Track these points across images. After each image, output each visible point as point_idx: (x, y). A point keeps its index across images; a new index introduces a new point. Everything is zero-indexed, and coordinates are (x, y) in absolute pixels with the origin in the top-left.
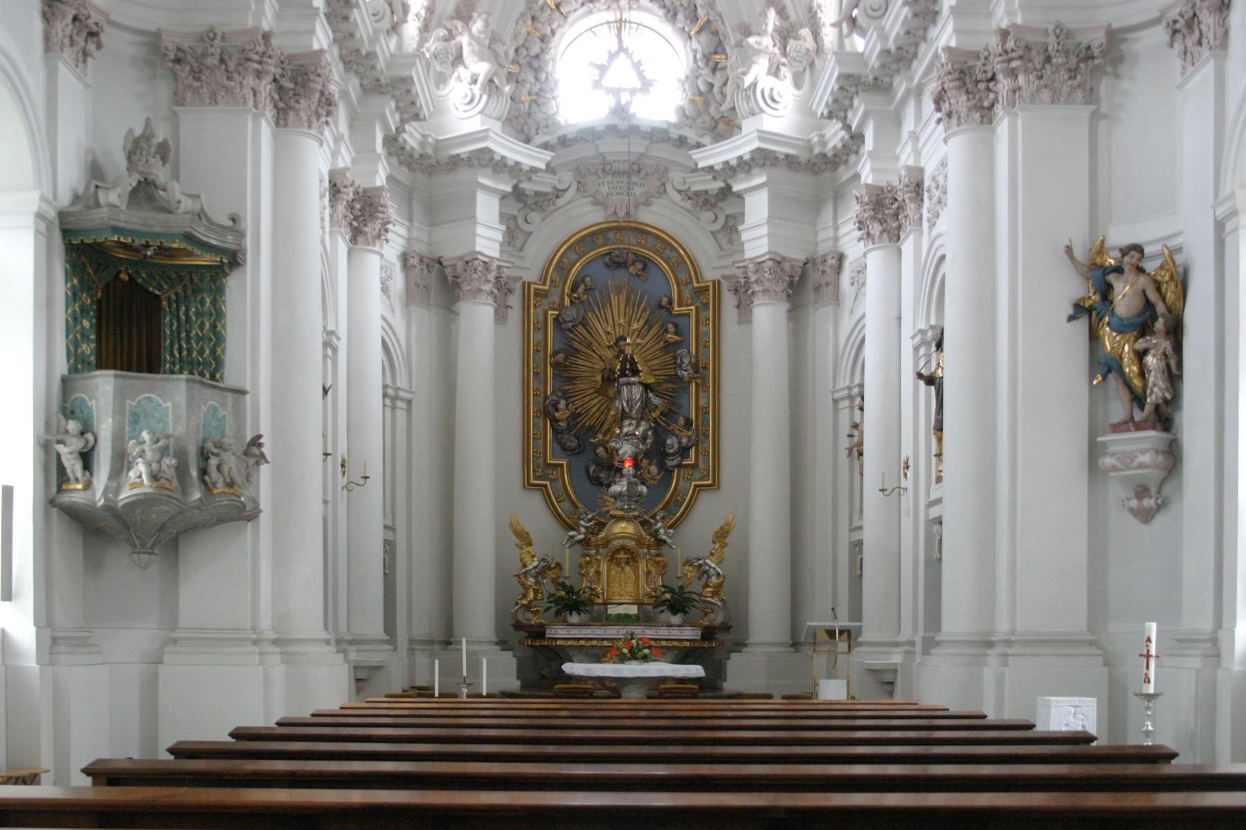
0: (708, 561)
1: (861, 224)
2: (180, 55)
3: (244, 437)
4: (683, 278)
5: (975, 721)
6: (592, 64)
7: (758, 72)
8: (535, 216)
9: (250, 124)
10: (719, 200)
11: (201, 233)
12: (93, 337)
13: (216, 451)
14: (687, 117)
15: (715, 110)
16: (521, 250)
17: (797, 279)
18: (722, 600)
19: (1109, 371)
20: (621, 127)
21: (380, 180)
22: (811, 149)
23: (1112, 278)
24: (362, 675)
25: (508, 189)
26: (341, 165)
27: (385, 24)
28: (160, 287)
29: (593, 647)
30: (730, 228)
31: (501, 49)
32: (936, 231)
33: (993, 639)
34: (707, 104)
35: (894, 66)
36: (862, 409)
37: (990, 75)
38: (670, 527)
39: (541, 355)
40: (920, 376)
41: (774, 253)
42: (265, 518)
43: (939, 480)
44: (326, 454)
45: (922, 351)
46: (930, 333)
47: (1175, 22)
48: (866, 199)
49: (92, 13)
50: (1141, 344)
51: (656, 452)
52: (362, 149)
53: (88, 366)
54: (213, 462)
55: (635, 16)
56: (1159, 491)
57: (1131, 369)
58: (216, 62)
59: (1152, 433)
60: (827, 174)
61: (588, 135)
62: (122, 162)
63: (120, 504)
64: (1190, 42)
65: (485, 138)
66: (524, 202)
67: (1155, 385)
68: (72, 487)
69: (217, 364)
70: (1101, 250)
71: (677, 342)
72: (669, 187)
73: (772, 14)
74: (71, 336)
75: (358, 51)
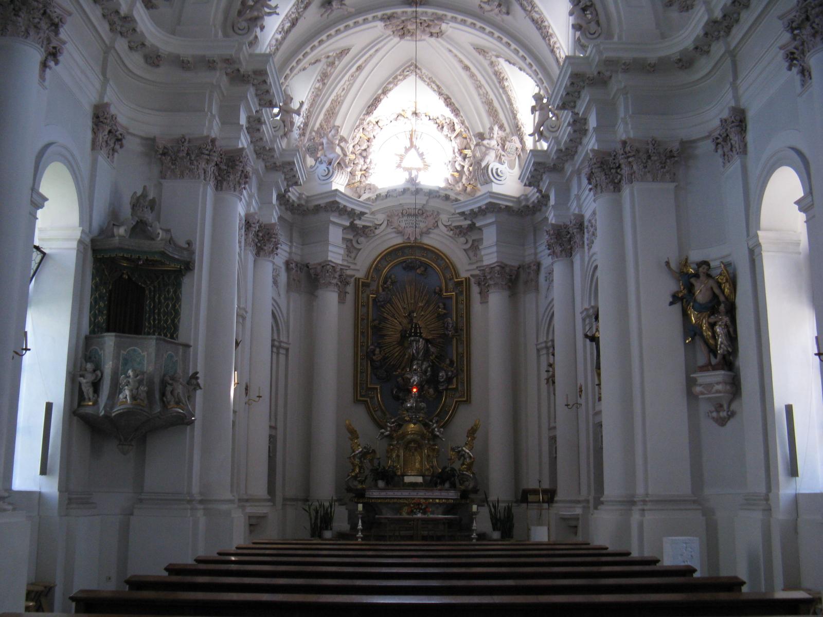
0: (464, 448)
1: (549, 247)
2: (166, 151)
4: (448, 276)
5: (623, 557)
6: (397, 155)
8: (362, 239)
9: (201, 190)
11: (170, 251)
12: (105, 312)
13: (171, 382)
14: (450, 184)
16: (355, 259)
17: (514, 277)
18: (473, 473)
19: (695, 334)
23: (693, 280)
24: (253, 521)
25: (348, 224)
26: (252, 210)
27: (281, 133)
29: (394, 503)
30: (475, 247)
32: (592, 251)
33: (635, 499)
35: (565, 158)
36: (553, 355)
37: (617, 165)
38: (442, 427)
39: (365, 321)
41: (502, 263)
42: (198, 425)
43: (600, 399)
45: (587, 321)
46: (591, 311)
47: (717, 138)
48: (552, 232)
49: (119, 129)
50: (712, 319)
51: (431, 381)
52: (264, 202)
54: (169, 388)
56: (729, 407)
58: (185, 155)
59: (722, 372)
63: (113, 415)
67: (722, 343)
68: (86, 403)
69: (174, 327)
70: (686, 263)
71: (445, 314)
73: (496, 128)
74: (92, 312)
75: (264, 147)
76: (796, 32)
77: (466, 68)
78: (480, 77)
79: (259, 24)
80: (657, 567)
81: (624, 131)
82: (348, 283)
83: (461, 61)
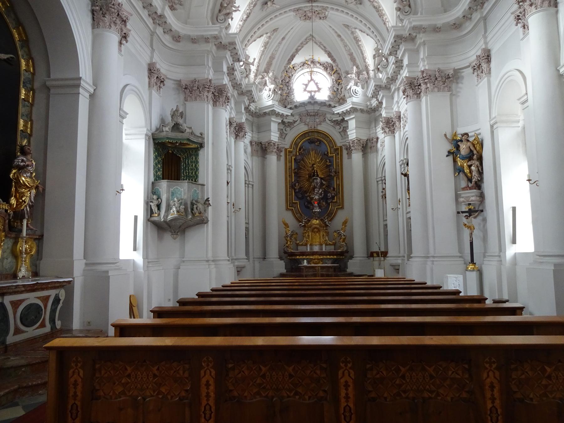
1: (383, 129)
3: (204, 198)
6: (303, 84)
7: (352, 84)
8: (288, 129)
10: (341, 123)
11: (192, 138)
15: (339, 96)
20: (312, 102)
21: (244, 120)
22: (367, 107)
23: (459, 143)
24: (239, 269)
26: (232, 116)
27: (245, 75)
28: (180, 155)
30: (345, 130)
31: (277, 81)
34: (337, 94)
40: (402, 174)
42: (210, 223)
43: (409, 205)
44: (228, 203)
45: (403, 166)
51: (325, 198)
52: (238, 112)
53: (160, 179)
54: (195, 206)
55: (315, 69)
57: (467, 171)
59: (475, 190)
60: (373, 114)
61: (303, 104)
62: (170, 118)
64: (479, 72)
65: (273, 107)
66: (285, 125)
70: (455, 135)
72: (326, 119)
73: (355, 68)
76: (521, 4)
77: (339, 36)
78: (346, 40)
79: (230, 16)
80: (441, 290)
81: (423, 66)
82: (281, 151)
83: (336, 32)
